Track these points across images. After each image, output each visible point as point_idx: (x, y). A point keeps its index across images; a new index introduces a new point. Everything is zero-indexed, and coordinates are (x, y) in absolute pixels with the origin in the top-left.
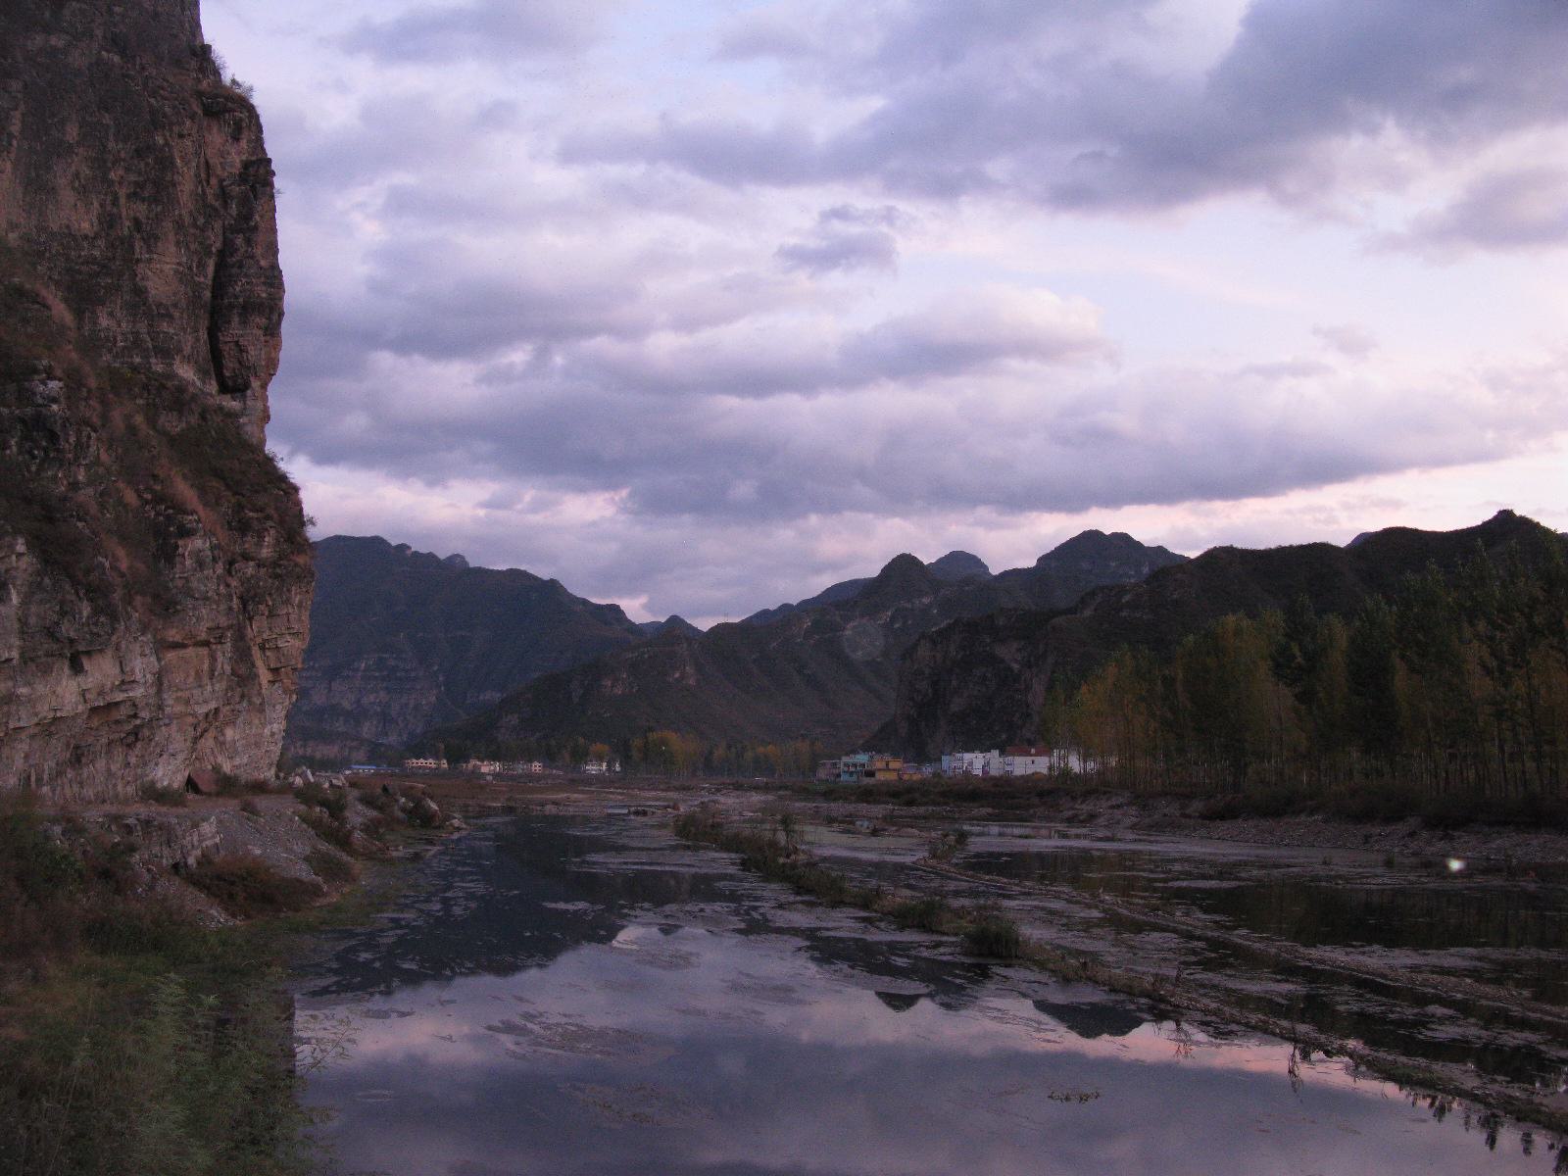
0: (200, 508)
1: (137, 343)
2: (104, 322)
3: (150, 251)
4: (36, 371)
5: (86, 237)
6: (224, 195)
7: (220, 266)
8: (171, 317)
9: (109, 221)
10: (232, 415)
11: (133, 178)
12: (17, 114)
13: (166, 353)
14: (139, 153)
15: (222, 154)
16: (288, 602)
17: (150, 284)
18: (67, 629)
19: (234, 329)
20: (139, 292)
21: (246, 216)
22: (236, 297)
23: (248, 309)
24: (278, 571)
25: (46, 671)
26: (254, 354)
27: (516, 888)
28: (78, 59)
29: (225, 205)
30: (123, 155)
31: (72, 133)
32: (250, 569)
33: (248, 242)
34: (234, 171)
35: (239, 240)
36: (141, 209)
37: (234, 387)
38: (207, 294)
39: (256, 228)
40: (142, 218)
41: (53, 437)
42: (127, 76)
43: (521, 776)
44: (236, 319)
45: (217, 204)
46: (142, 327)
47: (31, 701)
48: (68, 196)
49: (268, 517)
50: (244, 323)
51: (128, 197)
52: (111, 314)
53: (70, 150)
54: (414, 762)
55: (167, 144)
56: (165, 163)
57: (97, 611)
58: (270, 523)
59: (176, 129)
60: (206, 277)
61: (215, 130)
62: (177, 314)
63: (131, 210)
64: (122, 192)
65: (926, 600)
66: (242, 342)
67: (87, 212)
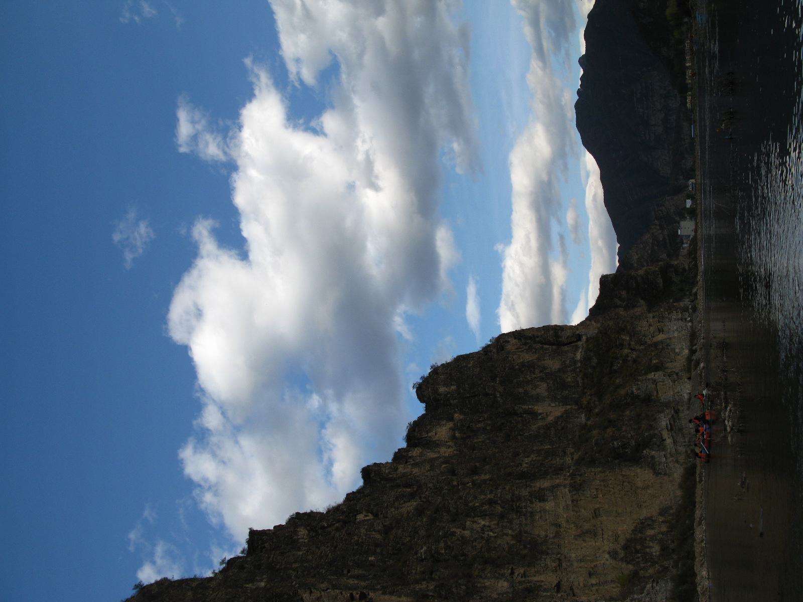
2: (569, 380)
4: (613, 447)
5: (548, 385)
6: (525, 344)
7: (546, 344)
9: (542, 379)
10: (588, 340)
13: (575, 362)
15: (514, 345)
18: (658, 443)
20: (559, 370)
21: (530, 338)
24: (632, 334)
26: (569, 333)
28: (501, 389)
29: (528, 343)
30: (523, 376)
31: (521, 390)
32: (633, 343)
35: (537, 339)
36: (537, 371)
37: (579, 338)
38: (554, 347)
44: (560, 339)
45: (528, 345)
48: (538, 390)
52: (567, 378)
54: (689, 105)
55: (518, 365)
58: (620, 337)
59: (513, 362)
61: (507, 347)
62: (563, 359)
64: (534, 376)
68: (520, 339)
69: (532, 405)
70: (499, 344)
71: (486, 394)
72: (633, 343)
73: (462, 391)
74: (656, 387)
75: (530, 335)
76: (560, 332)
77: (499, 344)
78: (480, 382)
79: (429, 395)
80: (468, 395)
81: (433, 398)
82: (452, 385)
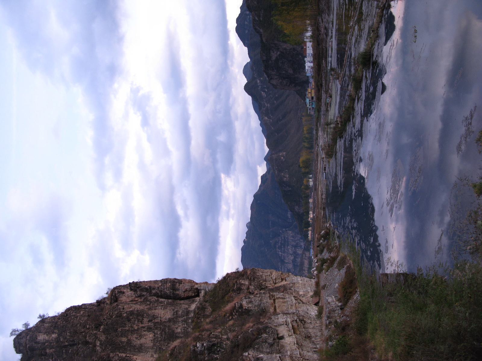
0: (234, 302)
1: (185, 321)
2: (179, 330)
3: (158, 317)
4: (194, 350)
5: (154, 336)
6: (140, 296)
7: (162, 297)
9: (149, 329)
10: (206, 293)
11: (136, 322)
13: (188, 312)
14: (129, 320)
15: (128, 297)
18: (270, 341)
19: (180, 293)
20: (170, 320)
24: (252, 279)
25: (283, 346)
26: (187, 286)
28: (103, 338)
29: (143, 296)
31: (124, 339)
32: (252, 287)
33: (154, 289)
35: (154, 291)
36: (145, 320)
38: (170, 300)
39: (150, 287)
41: (214, 345)
44: (177, 292)
46: (180, 319)
48: (143, 341)
49: (236, 282)
50: (178, 290)
51: (142, 323)
52: (177, 328)
53: (129, 340)
55: (126, 313)
56: (132, 313)
57: (265, 332)
59: (121, 310)
60: (165, 301)
62: (176, 309)
63: (146, 323)
64: (141, 325)
68: (135, 291)
69: (133, 354)
70: (114, 294)
71: (86, 343)
72: (252, 287)
73: (62, 340)
74: (275, 303)
75: (147, 286)
76: (178, 284)
77: (114, 294)
78: (83, 330)
79: (26, 343)
80: (67, 344)
81: (29, 347)
82: (53, 333)
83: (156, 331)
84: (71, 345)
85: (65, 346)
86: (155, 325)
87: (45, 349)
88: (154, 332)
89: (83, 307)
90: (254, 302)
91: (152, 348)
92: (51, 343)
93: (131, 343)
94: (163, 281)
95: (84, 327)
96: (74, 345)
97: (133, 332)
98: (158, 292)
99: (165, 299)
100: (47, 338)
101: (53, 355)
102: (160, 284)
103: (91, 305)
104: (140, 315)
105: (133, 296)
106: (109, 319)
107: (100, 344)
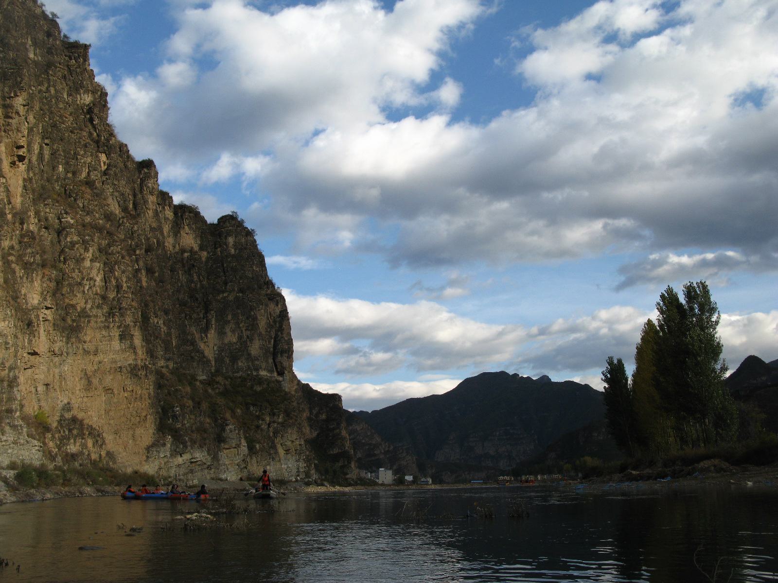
0: (231, 420)
1: (249, 368)
2: (240, 364)
3: (252, 343)
5: (234, 343)
6: (275, 322)
7: (275, 341)
8: (258, 359)
9: (240, 338)
11: (247, 325)
12: (214, 319)
13: (257, 370)
14: (247, 318)
16: (287, 432)
17: (252, 352)
19: (279, 358)
20: (249, 354)
21: (281, 326)
22: (279, 349)
23: (283, 352)
25: (175, 457)
26: (286, 364)
27: (640, 551)
28: (231, 298)
29: (275, 324)
31: (230, 317)
33: (282, 334)
34: (278, 314)
35: (279, 333)
36: (249, 333)
37: (281, 374)
38: (272, 349)
39: (283, 329)
40: (249, 335)
41: (177, 418)
42: (244, 299)
43: (63, 463)
46: (250, 364)
47: (173, 462)
48: (229, 334)
49: (281, 411)
50: (282, 356)
51: (245, 330)
52: (242, 362)
53: (229, 322)
56: (255, 319)
57: (183, 447)
59: (257, 309)
60: (271, 345)
63: (245, 334)
65: (764, 378)
66: (282, 361)
67: (235, 336)
68: (280, 316)
71: (226, 283)
73: (229, 259)
76: (287, 355)
81: (222, 231)
82: (235, 250)
83: (239, 344)
84: (224, 269)
85: (223, 265)
86: (244, 342)
87: (220, 246)
88: (237, 342)
89: (263, 269)
90: (231, 434)
91: (222, 343)
92: (226, 250)
93: (226, 324)
94: (290, 341)
95: (241, 278)
96: (224, 272)
97: (237, 324)
98: (279, 338)
99: (274, 345)
100: (231, 245)
101: (215, 255)
102: (286, 339)
103: (266, 274)
104: (253, 326)
105: (275, 314)
106: (248, 300)
107: (225, 297)
